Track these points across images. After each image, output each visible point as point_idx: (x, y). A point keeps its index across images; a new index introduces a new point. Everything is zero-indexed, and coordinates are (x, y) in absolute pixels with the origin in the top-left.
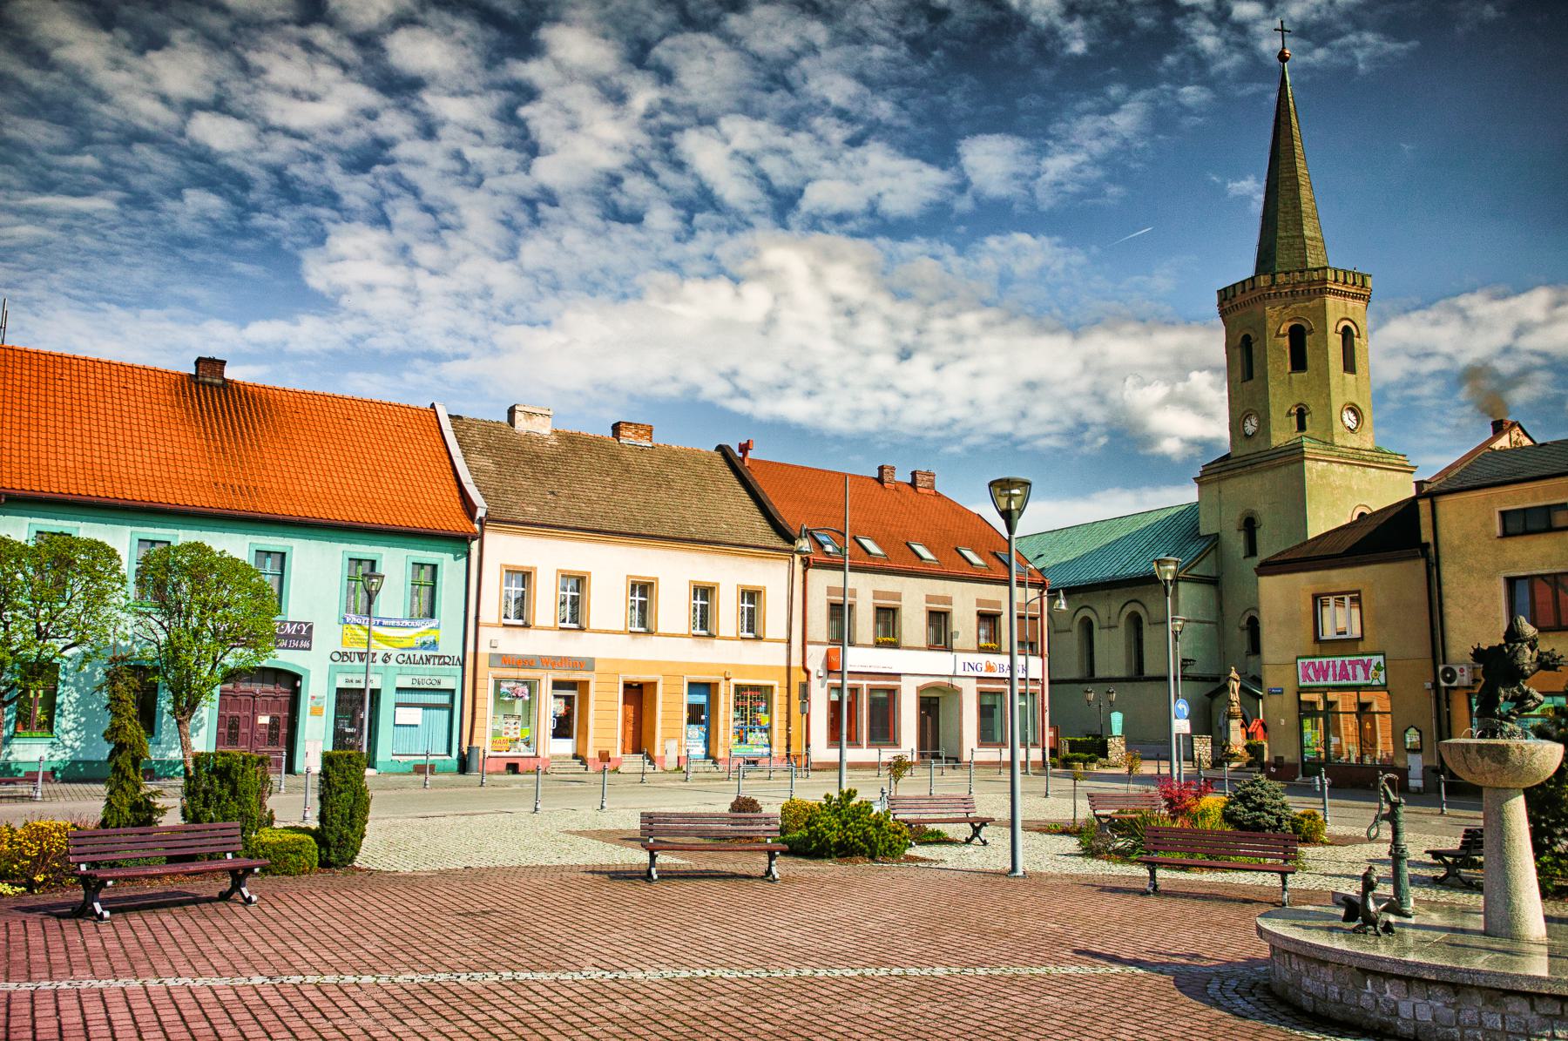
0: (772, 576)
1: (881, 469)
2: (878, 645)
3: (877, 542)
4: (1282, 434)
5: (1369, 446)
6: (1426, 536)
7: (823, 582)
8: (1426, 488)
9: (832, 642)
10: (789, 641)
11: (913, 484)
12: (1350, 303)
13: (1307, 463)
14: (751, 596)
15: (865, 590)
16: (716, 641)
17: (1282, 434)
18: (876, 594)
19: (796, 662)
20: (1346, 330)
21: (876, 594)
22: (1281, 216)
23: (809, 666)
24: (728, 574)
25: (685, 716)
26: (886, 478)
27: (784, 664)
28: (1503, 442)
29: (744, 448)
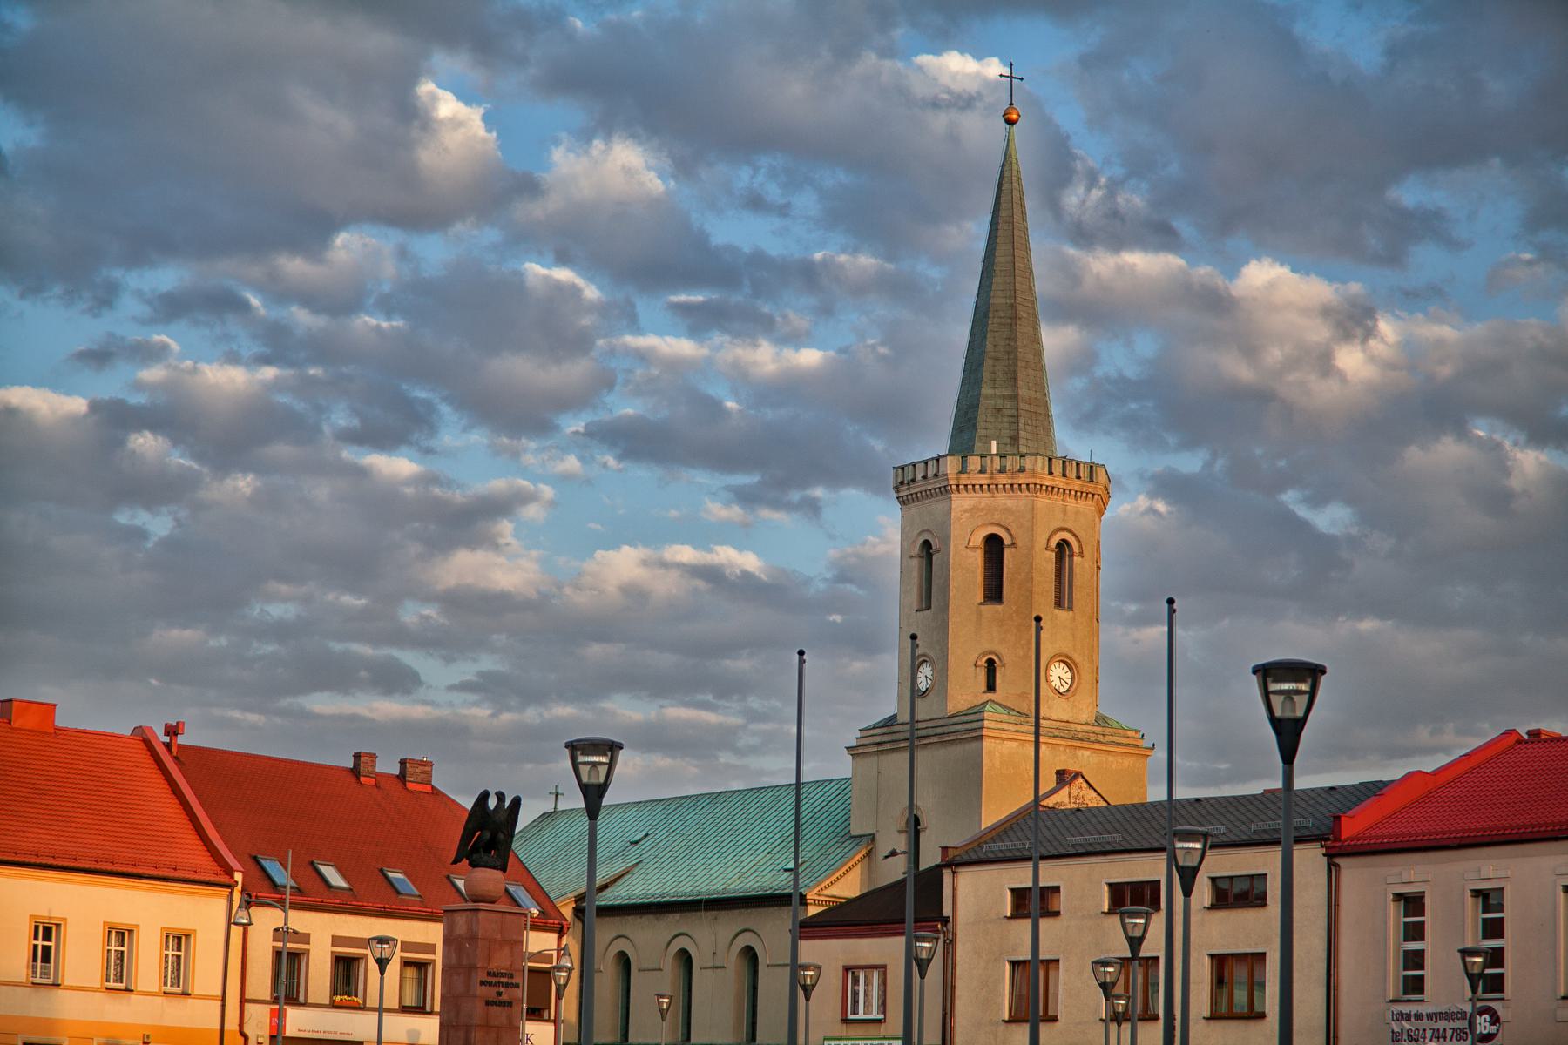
0: (204, 913)
1: (357, 756)
2: (334, 1006)
3: (341, 871)
4: (964, 691)
5: (1084, 717)
6: (947, 911)
7: (266, 920)
8: (951, 853)
9: (275, 1000)
10: (243, 1001)
11: (402, 777)
12: (1071, 503)
13: (987, 743)
14: (179, 938)
15: (322, 932)
16: (133, 997)
17: (964, 691)
18: (336, 940)
19: (232, 1024)
20: (1063, 546)
21: (336, 940)
22: (988, 363)
23: (246, 1030)
24: (150, 908)
25: (1428, 901)
26: (363, 770)
27: (217, 1027)
28: (1063, 799)
29: (173, 731)
